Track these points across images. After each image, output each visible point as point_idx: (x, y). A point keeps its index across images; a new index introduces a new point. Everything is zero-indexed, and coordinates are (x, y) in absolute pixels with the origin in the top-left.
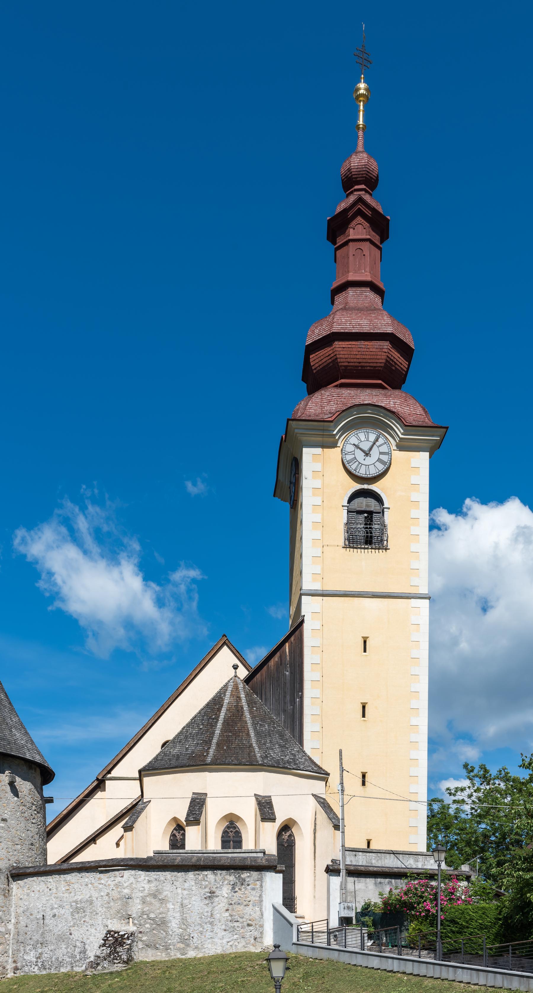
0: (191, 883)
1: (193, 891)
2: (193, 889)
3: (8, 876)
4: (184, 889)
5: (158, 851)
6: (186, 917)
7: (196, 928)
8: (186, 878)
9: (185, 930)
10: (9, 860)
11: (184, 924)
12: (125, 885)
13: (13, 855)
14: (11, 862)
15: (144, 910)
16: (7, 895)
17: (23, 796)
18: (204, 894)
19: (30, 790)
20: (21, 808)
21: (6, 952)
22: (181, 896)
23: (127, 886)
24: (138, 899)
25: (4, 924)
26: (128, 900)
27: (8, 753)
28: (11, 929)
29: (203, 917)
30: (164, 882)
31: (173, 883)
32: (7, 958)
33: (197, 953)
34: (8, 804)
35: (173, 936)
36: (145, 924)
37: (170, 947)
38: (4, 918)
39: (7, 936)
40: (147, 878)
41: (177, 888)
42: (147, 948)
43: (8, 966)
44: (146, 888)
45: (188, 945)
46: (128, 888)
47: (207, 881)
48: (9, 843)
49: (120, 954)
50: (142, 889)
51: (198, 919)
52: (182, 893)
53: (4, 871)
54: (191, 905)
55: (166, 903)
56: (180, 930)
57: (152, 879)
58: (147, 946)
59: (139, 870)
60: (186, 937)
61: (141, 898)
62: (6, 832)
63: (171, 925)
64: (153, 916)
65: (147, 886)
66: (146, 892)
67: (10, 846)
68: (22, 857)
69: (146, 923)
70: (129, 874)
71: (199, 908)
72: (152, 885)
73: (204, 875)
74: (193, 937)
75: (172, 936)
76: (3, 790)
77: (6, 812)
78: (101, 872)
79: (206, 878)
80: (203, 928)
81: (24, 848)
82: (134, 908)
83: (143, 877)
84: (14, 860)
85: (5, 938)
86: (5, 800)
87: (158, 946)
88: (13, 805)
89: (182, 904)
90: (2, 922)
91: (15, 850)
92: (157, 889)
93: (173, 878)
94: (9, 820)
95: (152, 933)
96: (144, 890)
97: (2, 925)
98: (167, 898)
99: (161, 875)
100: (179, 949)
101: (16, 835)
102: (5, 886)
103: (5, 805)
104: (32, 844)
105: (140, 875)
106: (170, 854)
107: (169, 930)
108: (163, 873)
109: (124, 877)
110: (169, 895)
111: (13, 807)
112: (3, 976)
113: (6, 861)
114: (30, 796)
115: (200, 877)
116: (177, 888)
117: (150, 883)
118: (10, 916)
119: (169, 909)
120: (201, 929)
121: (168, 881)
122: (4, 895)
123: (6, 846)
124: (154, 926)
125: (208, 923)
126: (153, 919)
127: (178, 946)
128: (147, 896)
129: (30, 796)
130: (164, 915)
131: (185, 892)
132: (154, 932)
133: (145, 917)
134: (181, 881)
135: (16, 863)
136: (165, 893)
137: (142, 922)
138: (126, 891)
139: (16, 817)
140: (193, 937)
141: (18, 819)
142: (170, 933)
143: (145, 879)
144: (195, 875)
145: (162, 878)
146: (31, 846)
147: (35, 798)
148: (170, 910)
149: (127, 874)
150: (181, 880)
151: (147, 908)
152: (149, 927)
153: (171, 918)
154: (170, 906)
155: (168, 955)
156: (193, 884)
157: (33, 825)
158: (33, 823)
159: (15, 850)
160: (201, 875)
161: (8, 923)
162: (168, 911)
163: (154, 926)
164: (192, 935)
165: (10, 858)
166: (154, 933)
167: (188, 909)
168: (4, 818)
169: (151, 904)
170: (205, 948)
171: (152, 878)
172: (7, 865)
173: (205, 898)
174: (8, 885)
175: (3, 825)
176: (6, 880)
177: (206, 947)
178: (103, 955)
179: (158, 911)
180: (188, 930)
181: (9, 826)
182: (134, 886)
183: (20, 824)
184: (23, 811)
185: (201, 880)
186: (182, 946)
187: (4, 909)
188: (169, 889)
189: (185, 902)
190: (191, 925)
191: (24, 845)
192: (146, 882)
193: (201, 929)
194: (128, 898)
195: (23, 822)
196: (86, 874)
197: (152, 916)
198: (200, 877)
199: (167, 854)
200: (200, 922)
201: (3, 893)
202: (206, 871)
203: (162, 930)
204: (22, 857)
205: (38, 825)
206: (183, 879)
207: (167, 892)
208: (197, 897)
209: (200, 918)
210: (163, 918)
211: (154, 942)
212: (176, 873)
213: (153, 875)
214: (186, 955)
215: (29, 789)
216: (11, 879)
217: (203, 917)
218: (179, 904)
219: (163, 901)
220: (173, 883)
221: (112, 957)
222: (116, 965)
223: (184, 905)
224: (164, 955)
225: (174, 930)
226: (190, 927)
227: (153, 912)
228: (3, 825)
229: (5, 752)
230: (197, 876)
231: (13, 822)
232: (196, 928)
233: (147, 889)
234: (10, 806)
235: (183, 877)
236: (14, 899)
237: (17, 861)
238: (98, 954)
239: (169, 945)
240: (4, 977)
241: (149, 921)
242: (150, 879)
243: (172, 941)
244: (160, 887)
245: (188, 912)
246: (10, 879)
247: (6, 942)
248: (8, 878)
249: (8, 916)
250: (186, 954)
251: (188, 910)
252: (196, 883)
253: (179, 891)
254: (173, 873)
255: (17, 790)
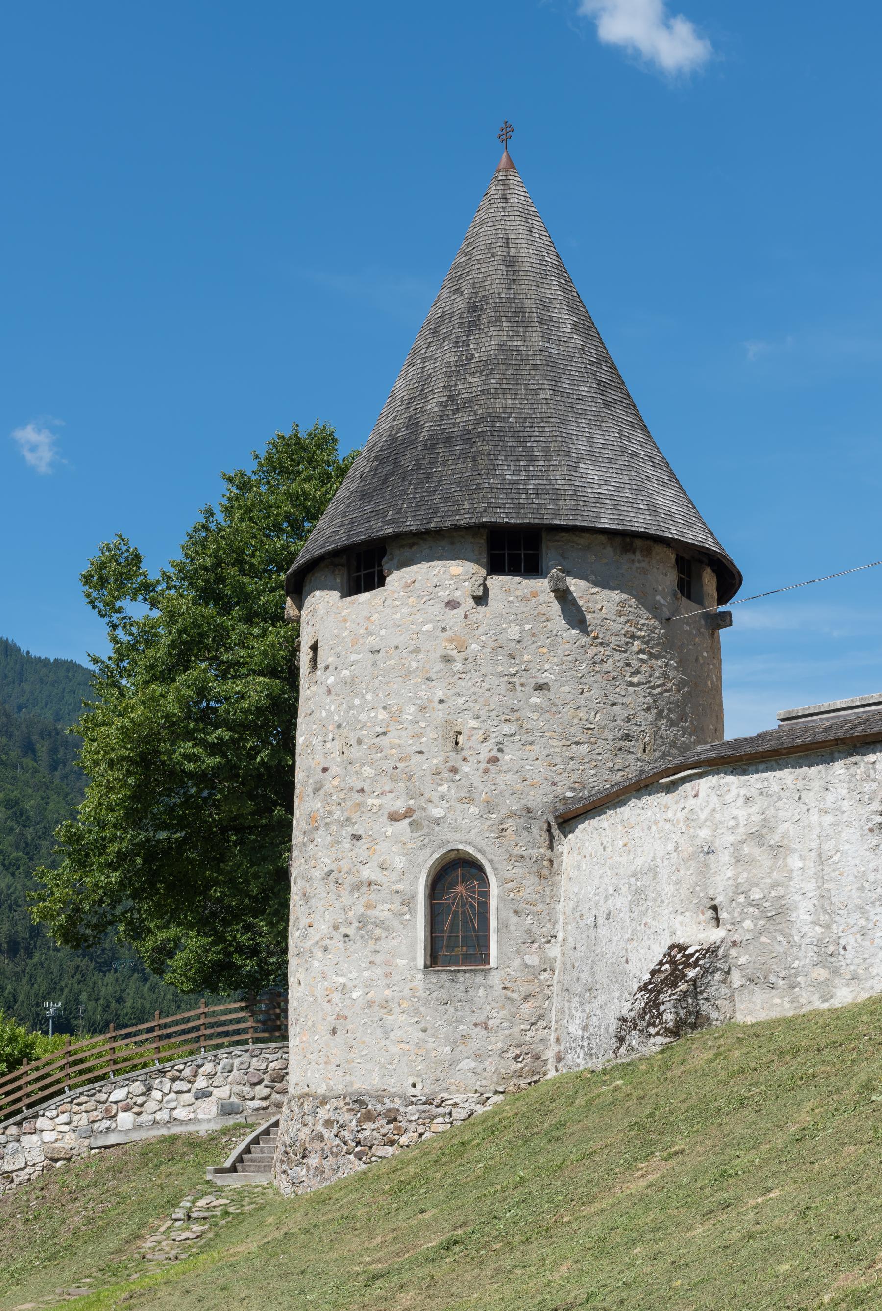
0: (839, 790)
1: (843, 813)
2: (844, 809)
3: (549, 824)
4: (825, 812)
5: (789, 712)
6: (829, 890)
7: (851, 921)
8: (829, 778)
9: (828, 927)
10: (554, 784)
11: (825, 911)
12: (703, 817)
13: (565, 770)
14: (559, 790)
15: (740, 880)
16: (545, 872)
17: (598, 622)
18: (869, 820)
19: (622, 604)
20: (592, 651)
21: (540, 1018)
22: (817, 831)
23: (706, 820)
24: (726, 851)
25: (536, 945)
26: (707, 857)
27: (546, 522)
28: (555, 958)
29: (867, 885)
30: (780, 798)
31: (800, 798)
32: (546, 1031)
33: (855, 993)
34: (553, 647)
35: (803, 947)
36: (743, 920)
37: (799, 979)
38: (539, 932)
39: (544, 976)
40: (743, 792)
41: (808, 810)
42: (752, 987)
43: (547, 1052)
44: (741, 819)
45: (835, 972)
46: (708, 823)
47: (874, 780)
48: (555, 743)
49: (662, 1008)
50: (732, 823)
51: (855, 894)
52: (820, 824)
53: (540, 813)
54: (839, 854)
55: (786, 856)
56: (817, 928)
57: (753, 792)
58: (750, 980)
59: (726, 773)
60: (831, 948)
61: (731, 849)
62: (547, 716)
63: (798, 917)
64: (757, 896)
65: (742, 814)
66: (742, 829)
67: (556, 750)
68: (593, 772)
69: (744, 916)
70: (708, 785)
71: (858, 862)
72: (755, 809)
73: (867, 763)
74: (844, 948)
75: (800, 946)
76: (540, 614)
77: (547, 667)
78: (671, 788)
79: (872, 771)
80: (868, 919)
81: (599, 750)
82: (718, 878)
83: (734, 792)
84: (568, 782)
85: (540, 981)
86: (542, 638)
87: (772, 979)
88: (568, 646)
89: (820, 855)
90: (533, 942)
91: (572, 759)
92: (765, 819)
93: (800, 784)
94: (554, 687)
95: (756, 944)
96: (738, 825)
97: (533, 950)
98: (786, 841)
99: (771, 779)
100: (817, 984)
101: (576, 721)
102: (541, 850)
103: (545, 650)
104: (627, 737)
105: (727, 784)
106: (814, 718)
107: (794, 932)
108: (778, 773)
109: (701, 795)
110: (791, 833)
111: (566, 653)
112: (535, 1078)
113: (546, 787)
114: (622, 619)
115: (859, 772)
116: (808, 810)
117: (750, 804)
118: (555, 923)
119: (791, 871)
120: (862, 922)
121: (787, 793)
122: (539, 874)
123: (547, 751)
124: (762, 923)
125: (877, 903)
126: (758, 906)
127: (815, 975)
128: (744, 841)
129: (622, 619)
130: (781, 891)
131: (828, 819)
132: (763, 939)
133: (741, 899)
134: (817, 789)
135: (573, 789)
136: (782, 828)
137: (736, 914)
138: (704, 833)
139: (574, 676)
140: (844, 948)
141: (583, 680)
142: (797, 939)
143: (739, 795)
144: (847, 769)
145: (775, 788)
146: (623, 743)
147: (642, 621)
148: (795, 874)
149: (706, 784)
150: (817, 785)
151: (745, 875)
152: (752, 927)
153: (797, 898)
154: (795, 862)
155: (795, 1004)
156: (845, 791)
157: (631, 689)
158: (631, 684)
159: (572, 759)
160: (863, 765)
161: (549, 942)
162: (791, 878)
163: (762, 923)
164: (843, 942)
165: (557, 779)
166: (762, 944)
167: (834, 867)
168: (541, 681)
169: (751, 861)
170: (873, 978)
171: (753, 790)
172: (549, 798)
173: (871, 830)
174: (551, 847)
175: (538, 700)
176: (546, 836)
177: (875, 972)
178: (632, 1014)
179: (768, 880)
180: (835, 926)
181: (556, 700)
182: (718, 816)
183: (589, 690)
184: (598, 658)
185: (862, 780)
186: (822, 973)
187: (538, 908)
188: (789, 814)
189: (828, 846)
190: (841, 912)
191: (600, 743)
192: (741, 801)
193: (862, 922)
194: (708, 853)
195: (596, 685)
196: (648, 798)
197: (756, 894)
198: (860, 771)
199: (810, 719)
200: (859, 902)
201: (535, 869)
202: (875, 753)
203: (780, 931)
204: (593, 772)
205: (653, 688)
206: (822, 783)
207: (786, 825)
208: (852, 830)
209: (858, 889)
210: (780, 897)
211: (764, 967)
212: (805, 769)
213: (755, 781)
214: (832, 1000)
215: (617, 601)
216: (558, 831)
217: (867, 885)
218: (814, 854)
219: (778, 850)
220: (800, 798)
221: (647, 1018)
222: (652, 1040)
223: (824, 857)
224: (787, 1005)
225: (805, 929)
226: (837, 919)
227: (757, 885)
228: (538, 700)
229: (537, 521)
230: (853, 769)
231: (567, 689)
232: (851, 921)
233: (742, 822)
234: (559, 651)
235: (821, 778)
236: (565, 886)
237: (577, 786)
238: (625, 1013)
239: (796, 975)
240: (535, 1082)
241: (751, 909)
242: (748, 795)
243: (802, 963)
244: (770, 812)
245: (833, 874)
246: (556, 832)
247: (542, 991)
248: (549, 830)
249: (549, 925)
250: (832, 997)
251: (834, 871)
252: (850, 791)
253: (814, 816)
254: (798, 771)
255: (578, 608)
